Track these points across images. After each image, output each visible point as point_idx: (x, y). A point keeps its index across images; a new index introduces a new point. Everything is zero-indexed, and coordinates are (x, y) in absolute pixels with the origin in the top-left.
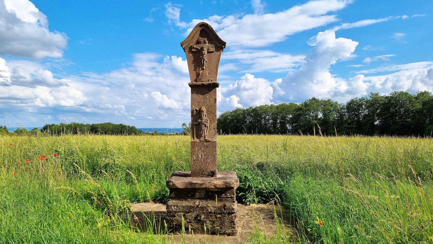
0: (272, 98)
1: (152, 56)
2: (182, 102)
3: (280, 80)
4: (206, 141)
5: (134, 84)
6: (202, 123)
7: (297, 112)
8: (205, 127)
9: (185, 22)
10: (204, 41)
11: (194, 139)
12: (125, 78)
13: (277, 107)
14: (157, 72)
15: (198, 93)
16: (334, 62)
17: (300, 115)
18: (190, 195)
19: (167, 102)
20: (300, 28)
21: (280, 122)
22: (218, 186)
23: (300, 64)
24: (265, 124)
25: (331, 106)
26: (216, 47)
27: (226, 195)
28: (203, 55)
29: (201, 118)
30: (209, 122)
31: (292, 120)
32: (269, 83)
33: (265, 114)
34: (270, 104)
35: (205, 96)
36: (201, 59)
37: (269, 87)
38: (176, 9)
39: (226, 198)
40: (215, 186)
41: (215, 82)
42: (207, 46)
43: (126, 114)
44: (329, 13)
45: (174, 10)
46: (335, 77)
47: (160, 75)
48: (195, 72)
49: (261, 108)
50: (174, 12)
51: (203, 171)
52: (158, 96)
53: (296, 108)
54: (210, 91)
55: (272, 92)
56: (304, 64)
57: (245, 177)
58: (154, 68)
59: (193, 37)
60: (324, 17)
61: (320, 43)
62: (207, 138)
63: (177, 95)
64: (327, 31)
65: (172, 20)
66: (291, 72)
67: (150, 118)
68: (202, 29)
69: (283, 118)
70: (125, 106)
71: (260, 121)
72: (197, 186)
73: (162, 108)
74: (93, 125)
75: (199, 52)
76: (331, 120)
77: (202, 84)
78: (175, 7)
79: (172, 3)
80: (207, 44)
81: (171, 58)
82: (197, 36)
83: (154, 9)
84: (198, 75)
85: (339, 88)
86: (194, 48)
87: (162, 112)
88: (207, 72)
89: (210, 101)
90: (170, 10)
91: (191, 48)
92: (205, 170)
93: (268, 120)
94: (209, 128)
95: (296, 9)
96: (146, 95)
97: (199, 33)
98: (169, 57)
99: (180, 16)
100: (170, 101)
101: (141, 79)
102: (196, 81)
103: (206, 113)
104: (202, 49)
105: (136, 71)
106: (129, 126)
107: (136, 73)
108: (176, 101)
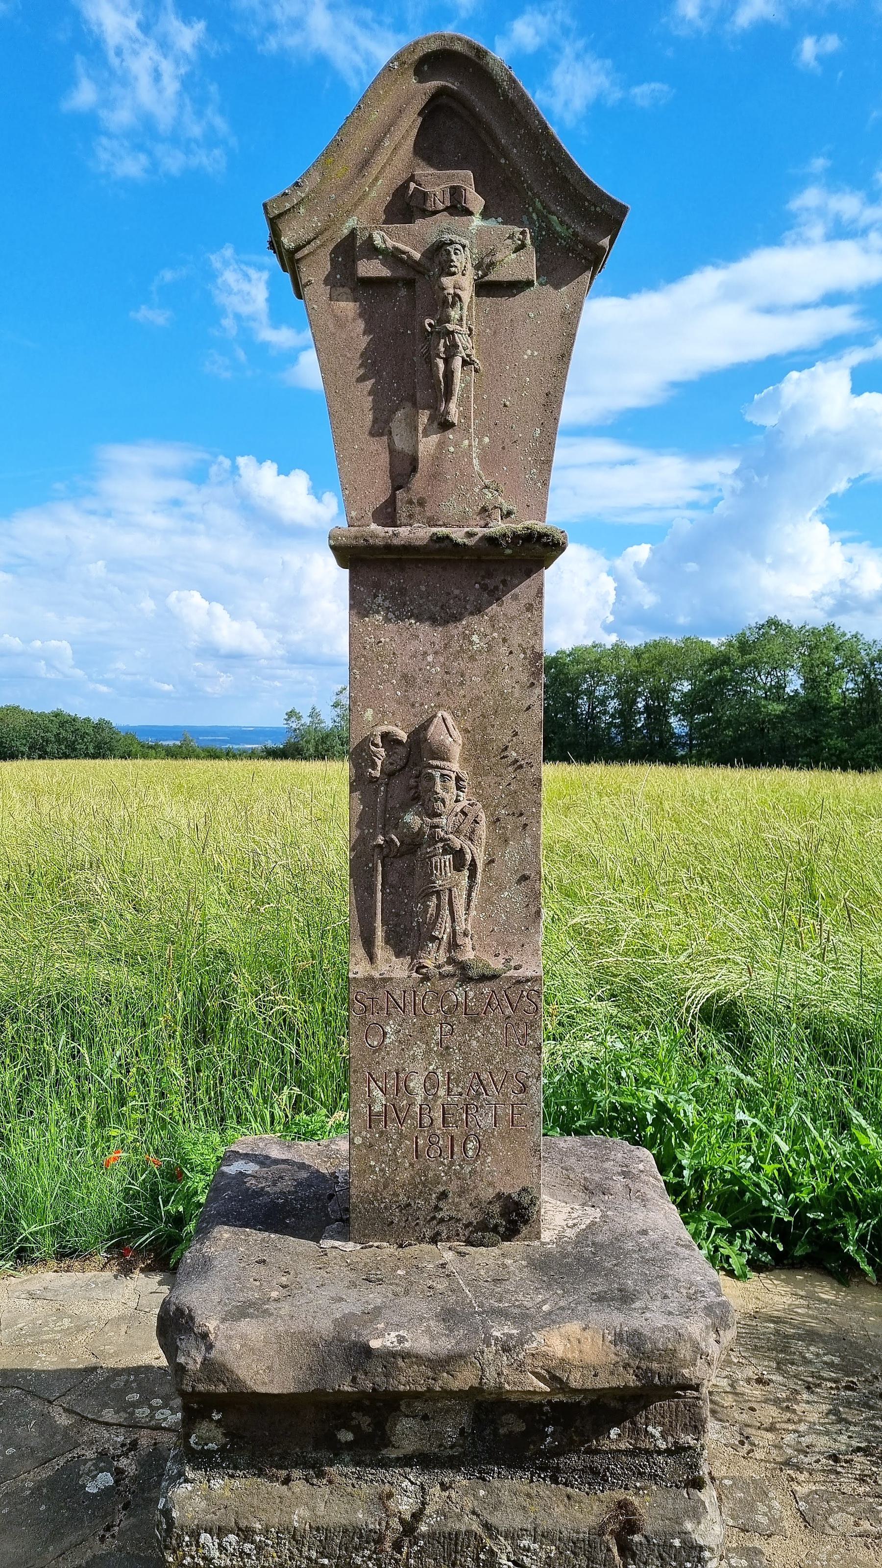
0: (611, 618)
1: (169, 456)
2: (283, 629)
3: (642, 552)
4: (464, 974)
5: (100, 563)
6: (433, 839)
7: (710, 670)
8: (458, 866)
9: (290, 326)
10: (456, 192)
11: (371, 957)
12: (67, 538)
13: (638, 654)
14: (191, 517)
15: (402, 609)
16: (840, 486)
17: (722, 681)
18: (346, 1436)
19: (228, 632)
20: (721, 356)
21: (647, 707)
22: (575, 1380)
23: (716, 494)
24: (592, 716)
25: (837, 649)
26: (546, 244)
27: (635, 1431)
28: (443, 303)
29: (421, 797)
30: (483, 830)
31: (692, 703)
32: (602, 562)
33: (593, 677)
34: (610, 640)
35: (455, 629)
36: (430, 337)
37: (604, 577)
38: (253, 273)
39: (633, 1453)
40: (553, 1379)
41: (539, 526)
42: (480, 238)
43: (79, 673)
44: (832, 299)
45: (247, 278)
46: (844, 542)
47: (201, 527)
48: (378, 448)
49: (577, 655)
50: (245, 287)
51: (443, 1195)
52: (193, 605)
53: (708, 655)
54: (495, 595)
55: (612, 598)
56: (733, 491)
57: (661, 1106)
58: (176, 503)
59: (365, 164)
60: (810, 312)
61: (795, 414)
62: (468, 955)
63: (263, 605)
64: (819, 368)
65: (238, 317)
66: (684, 523)
67: (167, 687)
68: (440, 93)
69: (660, 693)
70: (71, 644)
71: (572, 704)
72: (407, 1380)
73: (210, 651)
75: (410, 284)
76: (835, 700)
78: (248, 264)
79: (237, 251)
80: (476, 222)
81: (235, 469)
82: (397, 160)
83: (168, 275)
84: (403, 469)
85: (856, 582)
86: (372, 250)
87: (209, 667)
88: (469, 446)
89: (490, 673)
90: (230, 277)
91: (349, 250)
92: (453, 1187)
93: (603, 701)
94: (488, 878)
95: (706, 281)
96: (148, 605)
97: (409, 125)
98: (227, 463)
99: (268, 300)
100: (236, 626)
101: (128, 543)
103: (465, 760)
104: (439, 255)
105: (108, 514)
106: (88, 720)
107: (110, 521)
108: (259, 625)
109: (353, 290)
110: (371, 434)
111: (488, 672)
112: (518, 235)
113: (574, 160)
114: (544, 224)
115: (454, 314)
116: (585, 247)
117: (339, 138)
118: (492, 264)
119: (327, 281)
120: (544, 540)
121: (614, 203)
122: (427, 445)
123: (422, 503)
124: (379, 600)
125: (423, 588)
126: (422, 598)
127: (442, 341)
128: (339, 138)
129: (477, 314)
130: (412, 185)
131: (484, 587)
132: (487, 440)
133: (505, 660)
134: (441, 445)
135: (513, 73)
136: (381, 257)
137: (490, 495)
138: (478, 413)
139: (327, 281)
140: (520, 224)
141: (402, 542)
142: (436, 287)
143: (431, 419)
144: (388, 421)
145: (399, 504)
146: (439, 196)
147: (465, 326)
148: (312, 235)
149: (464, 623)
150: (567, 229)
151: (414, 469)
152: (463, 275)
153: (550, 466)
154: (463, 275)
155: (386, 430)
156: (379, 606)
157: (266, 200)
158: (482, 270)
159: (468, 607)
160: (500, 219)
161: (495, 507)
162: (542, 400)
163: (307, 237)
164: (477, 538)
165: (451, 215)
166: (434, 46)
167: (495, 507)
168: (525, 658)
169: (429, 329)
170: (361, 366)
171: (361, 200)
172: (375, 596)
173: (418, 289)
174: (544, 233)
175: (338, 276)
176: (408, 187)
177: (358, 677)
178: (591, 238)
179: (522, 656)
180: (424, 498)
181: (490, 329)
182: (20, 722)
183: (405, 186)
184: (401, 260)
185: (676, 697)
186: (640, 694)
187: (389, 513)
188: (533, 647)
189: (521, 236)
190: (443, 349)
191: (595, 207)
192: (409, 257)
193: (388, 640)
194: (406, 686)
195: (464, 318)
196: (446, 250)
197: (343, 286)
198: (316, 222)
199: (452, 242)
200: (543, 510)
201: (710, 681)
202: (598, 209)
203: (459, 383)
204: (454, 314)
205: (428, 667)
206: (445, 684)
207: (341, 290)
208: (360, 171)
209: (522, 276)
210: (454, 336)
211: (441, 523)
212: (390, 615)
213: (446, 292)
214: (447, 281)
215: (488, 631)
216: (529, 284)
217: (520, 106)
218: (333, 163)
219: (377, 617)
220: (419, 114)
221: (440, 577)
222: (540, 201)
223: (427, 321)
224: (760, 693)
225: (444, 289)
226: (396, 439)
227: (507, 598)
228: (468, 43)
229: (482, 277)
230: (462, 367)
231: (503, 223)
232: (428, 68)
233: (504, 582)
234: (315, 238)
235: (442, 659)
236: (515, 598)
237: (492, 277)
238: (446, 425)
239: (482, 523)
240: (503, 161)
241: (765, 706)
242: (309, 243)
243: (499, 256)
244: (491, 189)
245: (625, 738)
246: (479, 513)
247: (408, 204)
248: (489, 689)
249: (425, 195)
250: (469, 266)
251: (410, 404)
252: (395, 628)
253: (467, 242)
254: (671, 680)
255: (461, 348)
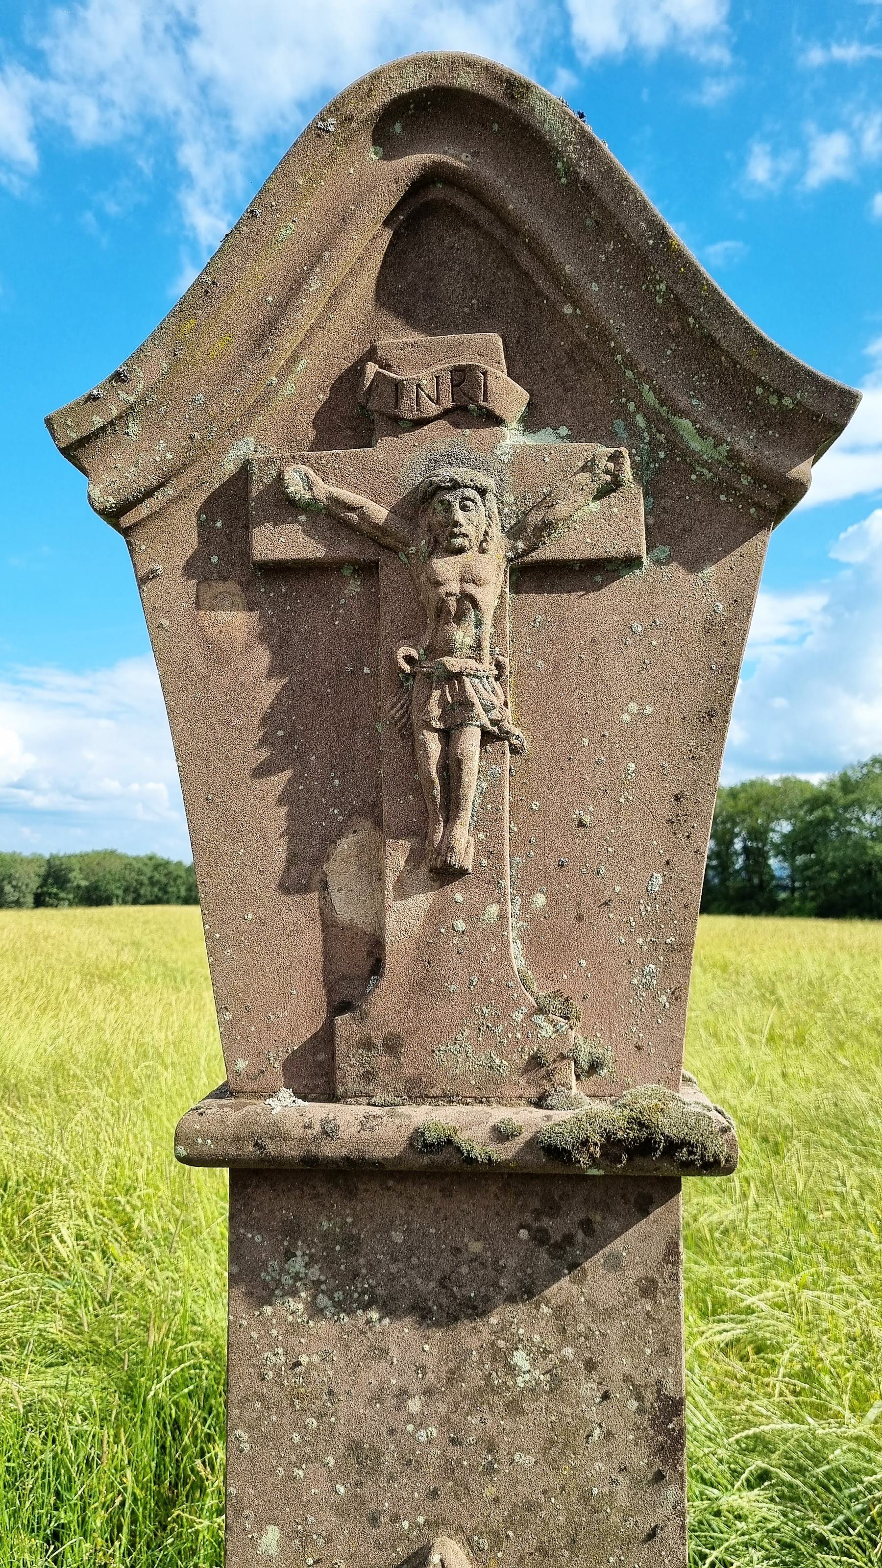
10: (464, 378)
15: (348, 1289)
17: (824, 821)
21: (745, 849)
28: (443, 613)
35: (474, 1336)
42: (518, 466)
48: (299, 915)
53: (808, 795)
54: (566, 1256)
59: (270, 327)
68: (429, 178)
69: (758, 834)
74: (53, 857)
75: (367, 570)
77: (420, 1143)
80: (512, 437)
82: (341, 312)
84: (354, 967)
86: (285, 506)
89: (559, 1444)
91: (236, 505)
97: (366, 243)
102: (316, 1073)
104: (428, 510)
109: (246, 586)
110: (285, 888)
111: (552, 1442)
112: (603, 463)
113: (729, 300)
114: (661, 437)
115: (462, 635)
116: (758, 480)
117: (209, 279)
118: (547, 526)
119: (189, 569)
120: (683, 1155)
121: (825, 388)
122: (406, 916)
123: (393, 1045)
124: (297, 1264)
125: (398, 1237)
126: (395, 1260)
127: (437, 694)
128: (209, 279)
129: (515, 631)
130: (372, 369)
131: (540, 1237)
132: (540, 900)
133: (593, 1414)
134: (437, 916)
135: (588, 128)
136: (302, 518)
137: (550, 1028)
138: (519, 842)
139: (189, 569)
140: (610, 438)
141: (344, 1152)
142: (423, 578)
143: (415, 858)
144: (320, 859)
145: (341, 1047)
146: (429, 387)
147: (487, 658)
148: (154, 480)
149: (493, 1320)
150: (715, 446)
151: (377, 968)
152: (483, 551)
153: (688, 957)
154: (483, 551)
155: (317, 878)
156: (296, 1277)
157: (50, 412)
158: (525, 540)
159: (502, 1282)
160: (564, 431)
161: (563, 1057)
162: (665, 810)
163: (143, 484)
164: (518, 1143)
165: (456, 425)
166: (414, 82)
167: (563, 1057)
168: (640, 1411)
169: (407, 668)
170: (263, 742)
171: (262, 402)
172: (289, 1255)
173: (383, 582)
174: (662, 455)
175: (215, 559)
176: (362, 373)
177: (246, 1447)
178: (771, 463)
179: (633, 1404)
180: (398, 1037)
181: (545, 661)
182: (116, 866)
183: (356, 371)
184: (347, 524)
185: (775, 837)
186: (737, 835)
187: (320, 1065)
188: (659, 1382)
189: (611, 465)
190: (436, 712)
191: (781, 396)
192: (363, 516)
193: (316, 1359)
194: (359, 1473)
195: (486, 644)
196: (442, 502)
197: (225, 580)
198: (164, 452)
199: (456, 485)
200: (674, 1058)
201: (811, 822)
202: (787, 401)
203: (474, 781)
204: (462, 635)
205: (410, 1427)
206: (449, 1469)
207: (220, 587)
208: (258, 343)
209: (616, 548)
210: (461, 683)
211: (436, 1091)
212: (323, 1300)
213: (442, 590)
214: (446, 568)
215: (551, 1342)
216: (631, 562)
217: (605, 194)
218: (196, 329)
219: (293, 1304)
220: (386, 223)
221: (437, 1211)
222: (652, 388)
223: (402, 651)
224: (866, 833)
225: (438, 584)
226: (338, 899)
227: (594, 1264)
228: (488, 70)
229: (525, 553)
230: (483, 744)
231: (570, 438)
232: (404, 128)
233: (587, 1226)
234: (161, 485)
235: (443, 1408)
236: (614, 1263)
237: (547, 552)
238: (446, 874)
239: (533, 1092)
240: (568, 310)
241: (872, 848)
242: (149, 493)
243: (562, 509)
244: (543, 369)
245: (723, 881)
246: (526, 1071)
247: (363, 408)
248: (556, 1483)
249: (398, 387)
250: (496, 532)
251: (368, 824)
252: (334, 1331)
253: (489, 482)
254: (769, 819)
255: (478, 709)
